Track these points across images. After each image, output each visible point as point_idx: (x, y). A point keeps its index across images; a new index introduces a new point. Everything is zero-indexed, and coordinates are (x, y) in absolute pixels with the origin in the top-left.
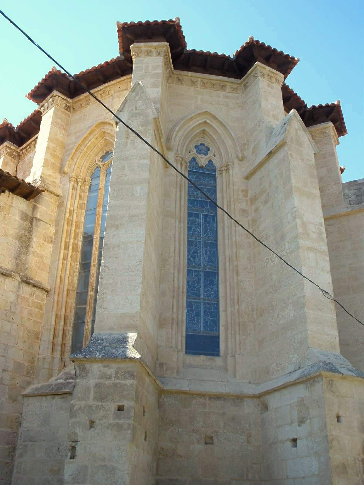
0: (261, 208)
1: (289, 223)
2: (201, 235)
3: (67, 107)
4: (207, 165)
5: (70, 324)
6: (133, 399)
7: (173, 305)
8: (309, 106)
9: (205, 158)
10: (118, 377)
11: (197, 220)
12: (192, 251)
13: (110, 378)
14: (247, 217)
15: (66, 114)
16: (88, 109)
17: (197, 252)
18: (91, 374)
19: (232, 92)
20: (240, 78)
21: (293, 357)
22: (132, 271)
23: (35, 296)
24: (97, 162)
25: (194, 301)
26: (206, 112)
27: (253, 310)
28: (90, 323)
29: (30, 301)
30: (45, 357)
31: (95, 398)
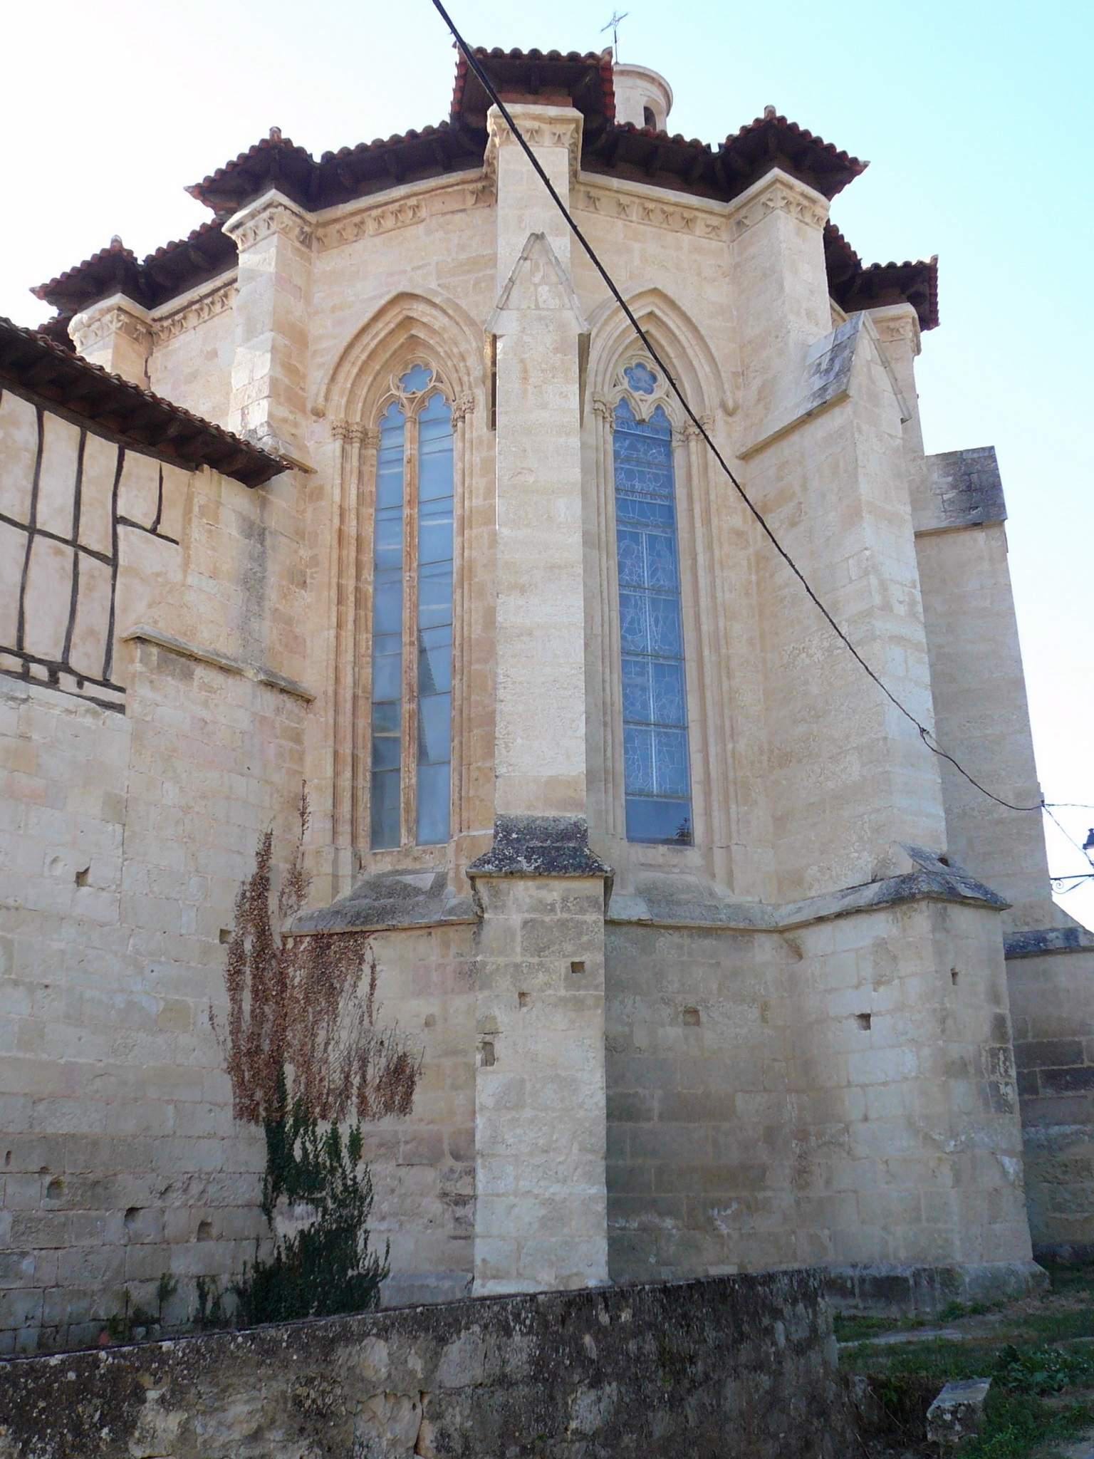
1: (851, 581)
4: (651, 417)
5: (364, 775)
7: (605, 742)
8: (866, 265)
11: (635, 547)
12: (629, 618)
13: (553, 910)
14: (745, 548)
16: (359, 246)
17: (639, 620)
21: (859, 858)
24: (394, 391)
26: (655, 291)
27: (762, 753)
29: (277, 725)
31: (525, 950)
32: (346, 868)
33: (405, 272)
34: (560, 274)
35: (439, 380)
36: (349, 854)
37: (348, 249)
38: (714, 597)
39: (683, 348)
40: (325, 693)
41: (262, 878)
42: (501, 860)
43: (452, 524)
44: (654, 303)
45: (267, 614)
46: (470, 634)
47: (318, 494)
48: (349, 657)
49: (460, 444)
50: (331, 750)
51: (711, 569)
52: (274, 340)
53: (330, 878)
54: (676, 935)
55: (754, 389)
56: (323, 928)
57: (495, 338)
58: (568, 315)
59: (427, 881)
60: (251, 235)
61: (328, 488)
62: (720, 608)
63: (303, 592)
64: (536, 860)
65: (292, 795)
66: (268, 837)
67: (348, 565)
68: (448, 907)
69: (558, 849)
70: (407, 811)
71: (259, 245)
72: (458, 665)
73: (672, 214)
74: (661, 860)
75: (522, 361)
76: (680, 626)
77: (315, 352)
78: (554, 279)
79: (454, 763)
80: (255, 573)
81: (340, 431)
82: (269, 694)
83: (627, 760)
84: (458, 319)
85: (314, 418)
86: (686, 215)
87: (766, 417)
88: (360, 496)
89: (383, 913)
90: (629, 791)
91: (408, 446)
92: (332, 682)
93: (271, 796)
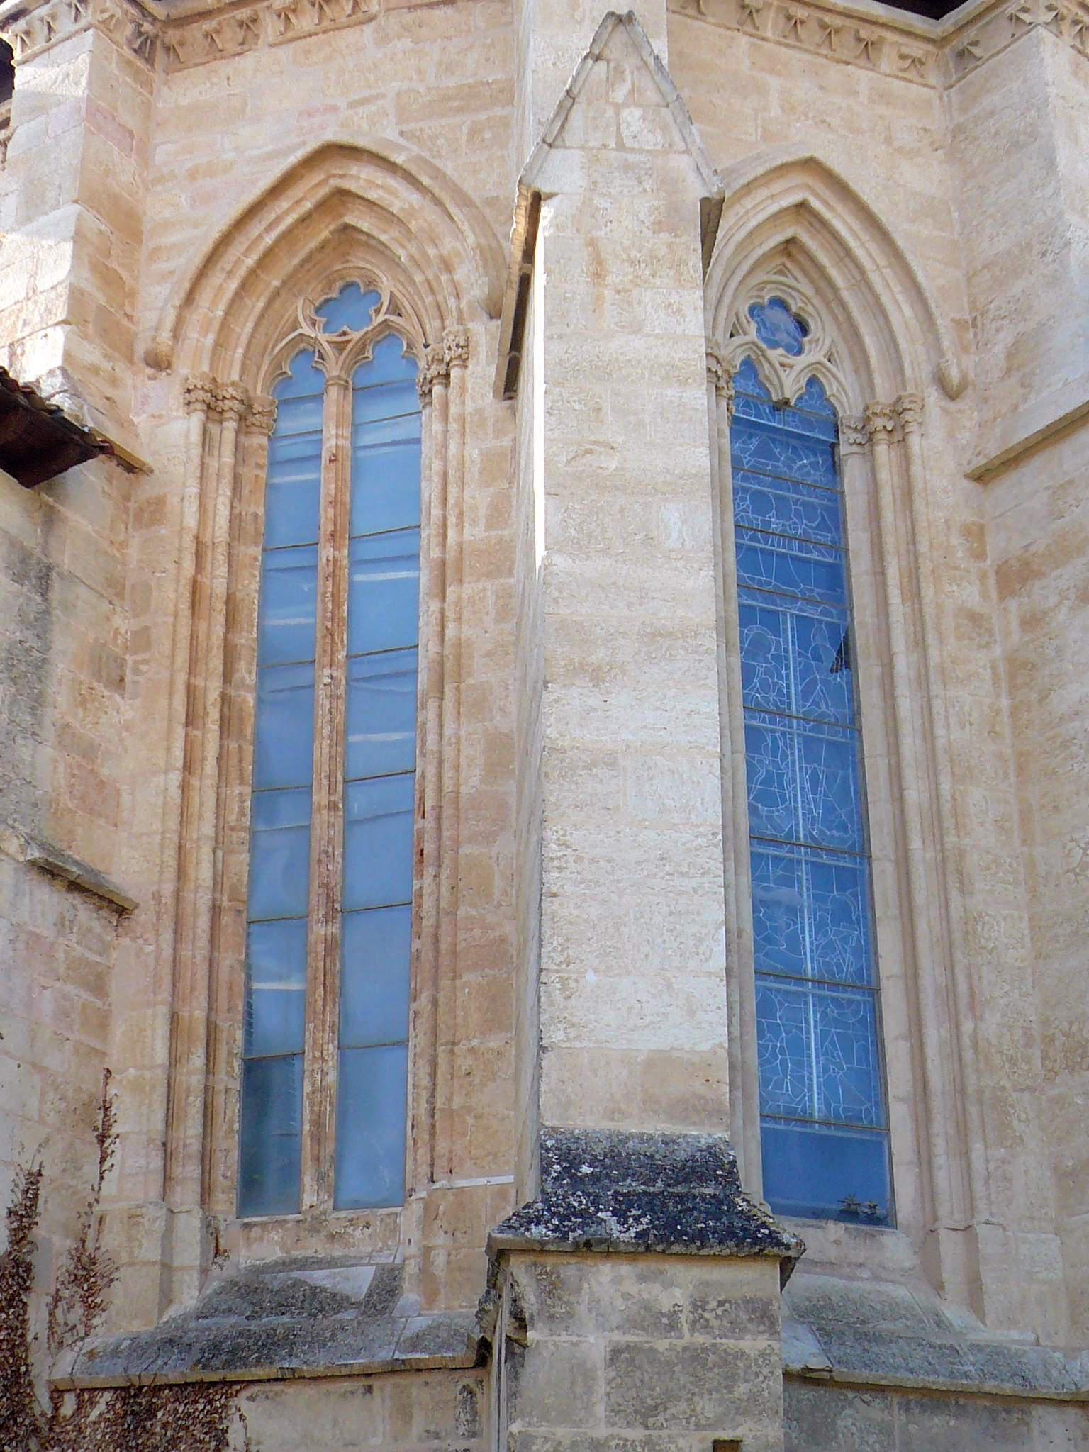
0: (1062, 615)
2: (789, 704)
3: (139, 41)
4: (800, 398)
6: (777, 1412)
9: (797, 368)
10: (707, 1321)
12: (762, 774)
13: (673, 1326)
14: (987, 645)
15: (136, 73)
16: (247, 62)
17: (780, 776)
18: (590, 1310)
19: (900, 74)
20: (937, 16)
22: (683, 874)
23: (75, 929)
24: (306, 330)
25: (778, 991)
26: (811, 165)
28: (330, 1064)
30: (139, 1212)
32: (190, 1251)
33: (334, 109)
34: (666, 87)
35: (396, 309)
36: (196, 1222)
37: (224, 67)
38: (928, 735)
39: (862, 272)
40: (157, 897)
41: (17, 1264)
42: (563, 1218)
43: (419, 578)
44: (809, 188)
45: (49, 734)
46: (457, 785)
47: (153, 512)
48: (208, 829)
49: (437, 427)
50: (163, 1010)
51: (922, 681)
52: (80, 218)
53: (156, 1270)
54: (877, 1403)
55: (999, 349)
56: (140, 1372)
57: (537, 200)
58: (682, 164)
59: (359, 1281)
60: (41, 32)
61: (173, 501)
62: (942, 759)
63: (117, 698)
64: (637, 1219)
65: (85, 1097)
66: (34, 1178)
67: (208, 651)
68: (408, 1333)
69: (680, 1198)
70: (318, 1139)
71: (56, 50)
72: (429, 848)
73: (837, 31)
74: (832, 1253)
75: (592, 243)
76: (862, 794)
77: (158, 249)
78: (652, 96)
79: (418, 1040)
80: (28, 650)
81: (200, 395)
82: (47, 889)
83: (762, 1050)
84: (437, 191)
85: (150, 371)
86: (863, 34)
87: (1025, 399)
88: (235, 520)
89: (269, 1345)
90: (767, 1111)
91: (330, 431)
92: (171, 873)
93: (43, 1094)
